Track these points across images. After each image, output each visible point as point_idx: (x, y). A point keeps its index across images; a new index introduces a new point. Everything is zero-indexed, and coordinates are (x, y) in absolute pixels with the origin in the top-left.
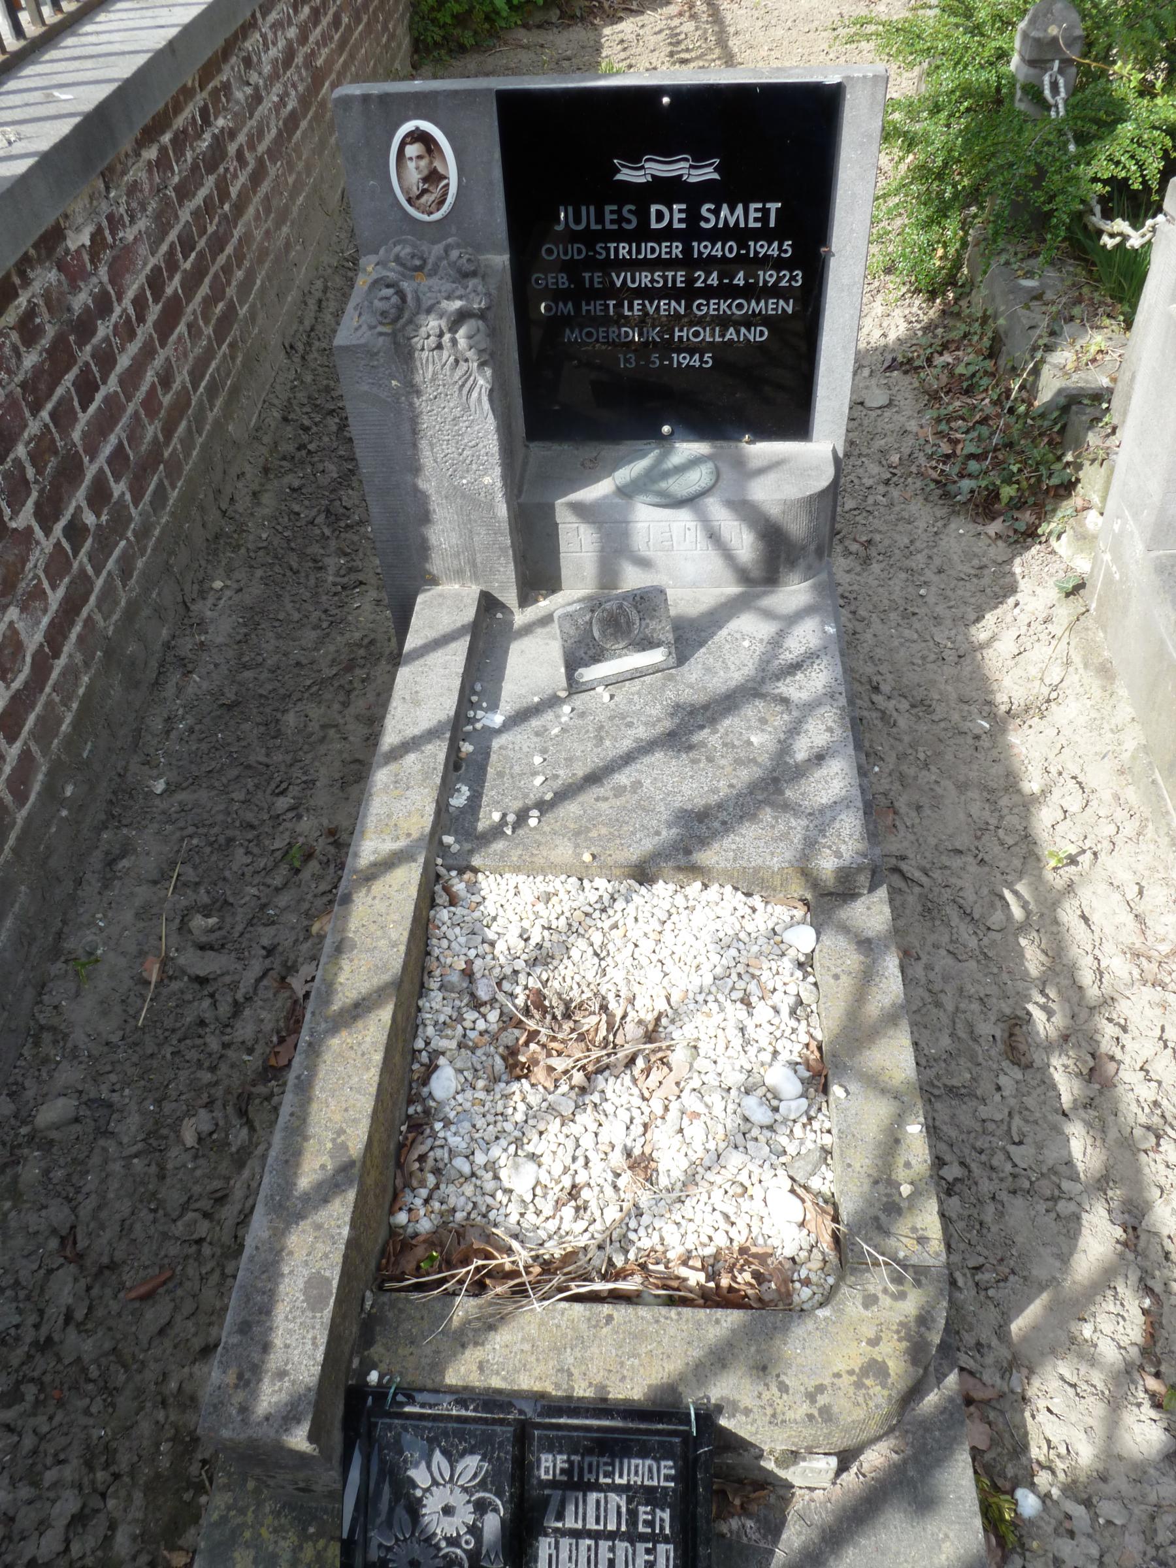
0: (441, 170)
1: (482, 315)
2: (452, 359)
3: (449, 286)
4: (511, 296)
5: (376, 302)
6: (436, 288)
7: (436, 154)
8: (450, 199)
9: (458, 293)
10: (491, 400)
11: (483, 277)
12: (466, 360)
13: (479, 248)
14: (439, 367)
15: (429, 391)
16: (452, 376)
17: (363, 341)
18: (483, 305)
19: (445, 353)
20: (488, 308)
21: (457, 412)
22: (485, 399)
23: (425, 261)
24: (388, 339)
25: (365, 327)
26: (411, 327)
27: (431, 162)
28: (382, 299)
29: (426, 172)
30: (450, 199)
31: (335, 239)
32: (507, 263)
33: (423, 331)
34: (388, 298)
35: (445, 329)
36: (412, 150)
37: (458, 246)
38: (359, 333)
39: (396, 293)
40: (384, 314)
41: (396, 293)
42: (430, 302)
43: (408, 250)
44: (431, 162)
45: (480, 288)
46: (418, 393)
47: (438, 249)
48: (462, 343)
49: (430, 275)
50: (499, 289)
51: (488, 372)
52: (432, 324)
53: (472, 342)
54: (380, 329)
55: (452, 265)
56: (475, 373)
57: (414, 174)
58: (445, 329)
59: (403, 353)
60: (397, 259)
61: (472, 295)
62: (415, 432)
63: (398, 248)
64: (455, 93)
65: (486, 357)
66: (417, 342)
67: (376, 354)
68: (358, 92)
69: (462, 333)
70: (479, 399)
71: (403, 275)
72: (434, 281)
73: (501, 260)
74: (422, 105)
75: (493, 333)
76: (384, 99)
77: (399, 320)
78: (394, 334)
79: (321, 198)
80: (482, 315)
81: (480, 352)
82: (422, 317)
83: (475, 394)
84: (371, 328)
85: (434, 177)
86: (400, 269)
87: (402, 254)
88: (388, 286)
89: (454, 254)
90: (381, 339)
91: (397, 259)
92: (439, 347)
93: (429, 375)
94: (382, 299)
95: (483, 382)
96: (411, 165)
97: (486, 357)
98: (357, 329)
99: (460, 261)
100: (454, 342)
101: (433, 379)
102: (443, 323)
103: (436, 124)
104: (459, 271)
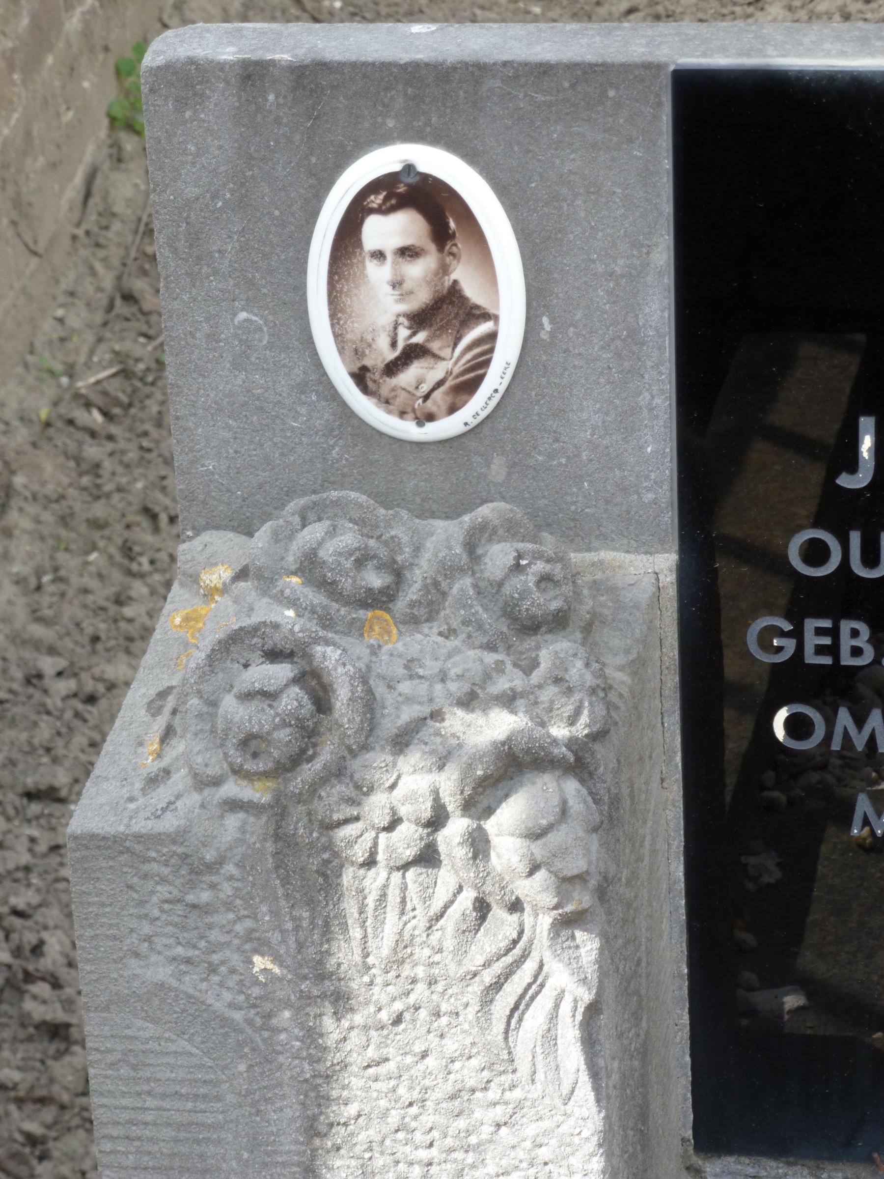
0: (473, 291)
1: (578, 762)
2: (467, 898)
3: (471, 660)
4: (673, 681)
5: (229, 702)
6: (431, 667)
7: (461, 245)
8: (496, 378)
9: (502, 684)
10: (590, 1041)
11: (587, 629)
12: (516, 906)
13: (578, 530)
14: (421, 922)
15: (377, 997)
16: (461, 952)
17: (169, 823)
18: (581, 728)
19: (446, 879)
20: (598, 736)
21: (468, 1073)
22: (569, 1035)
23: (398, 574)
24: (258, 825)
25: (180, 779)
26: (340, 789)
27: (444, 269)
28: (247, 696)
29: (422, 298)
30: (496, 378)
31: (48, 326)
32: (669, 579)
33: (377, 807)
34: (269, 696)
35: (452, 803)
36: (385, 230)
37: (510, 529)
38: (163, 794)
39: (299, 680)
40: (250, 743)
41: (299, 680)
42: (408, 714)
43: (348, 539)
44: (444, 269)
45: (577, 671)
46: (341, 1001)
47: (444, 536)
48: (507, 848)
49: (412, 621)
50: (637, 666)
51: (588, 945)
52: (411, 783)
53: (538, 849)
54: (232, 788)
55: (491, 591)
56: (542, 949)
57: (384, 300)
58: (452, 803)
59: (303, 871)
60: (310, 566)
61: (549, 693)
62: (314, 1129)
63: (315, 532)
64: (543, 71)
65: (582, 899)
66: (355, 839)
67: (212, 867)
68: (228, 53)
69: (509, 816)
70: (550, 1038)
71: (326, 621)
72: (424, 642)
73: (650, 569)
74: (430, 98)
75: (612, 818)
76: (311, 80)
77: (302, 761)
78: (279, 809)
79: (18, 202)
80: (578, 762)
81: (566, 883)
82: (379, 758)
83: (535, 1018)
84: (204, 782)
85: (446, 311)
86: (315, 597)
87: (326, 553)
88: (274, 655)
89: (498, 556)
90: (233, 821)
91: (310, 566)
92: (428, 857)
93: (383, 947)
94: (247, 696)
95: (569, 975)
96: (378, 275)
97: (582, 899)
98: (153, 782)
99: (517, 583)
100: (479, 845)
101: (396, 961)
102: (448, 784)
103: (471, 157)
104: (510, 612)
